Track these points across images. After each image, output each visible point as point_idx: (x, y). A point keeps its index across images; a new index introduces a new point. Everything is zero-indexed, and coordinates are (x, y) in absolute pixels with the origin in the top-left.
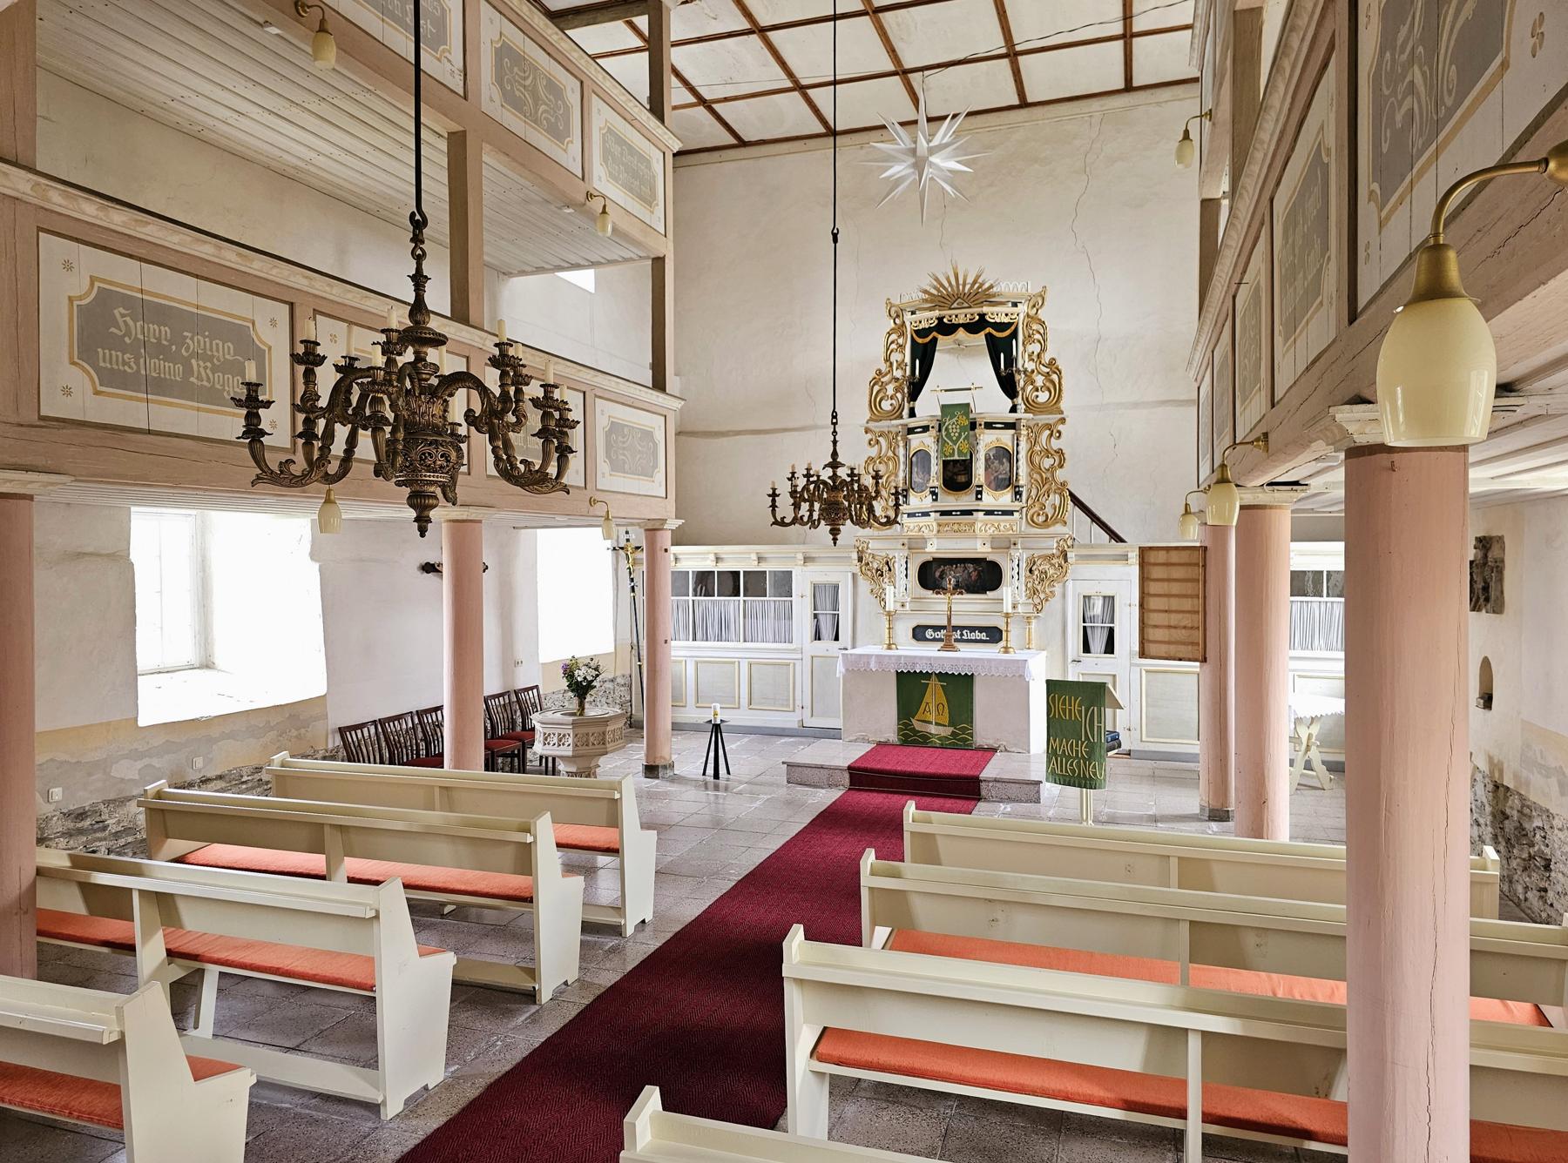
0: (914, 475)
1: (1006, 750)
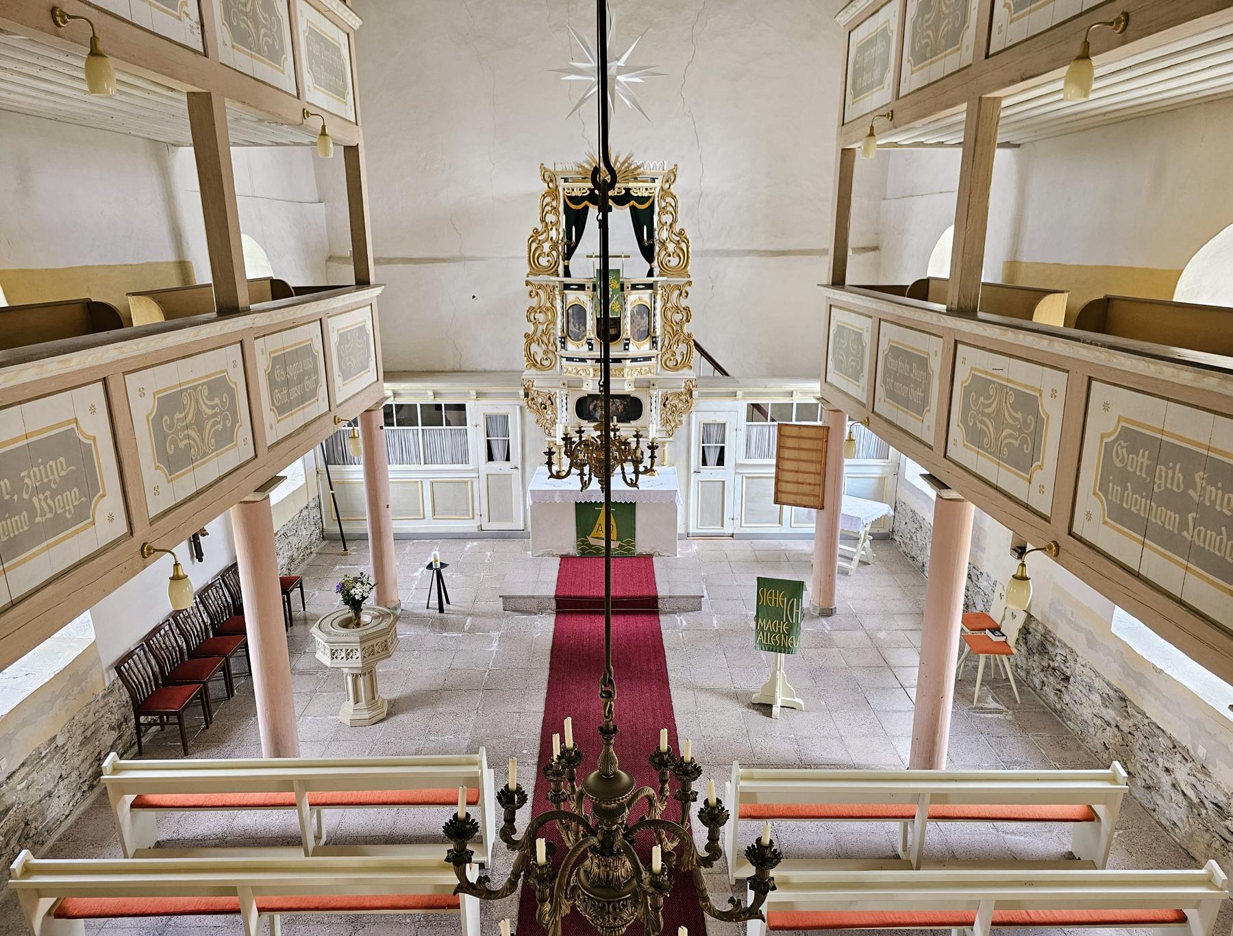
0: (571, 325)
1: (659, 555)
